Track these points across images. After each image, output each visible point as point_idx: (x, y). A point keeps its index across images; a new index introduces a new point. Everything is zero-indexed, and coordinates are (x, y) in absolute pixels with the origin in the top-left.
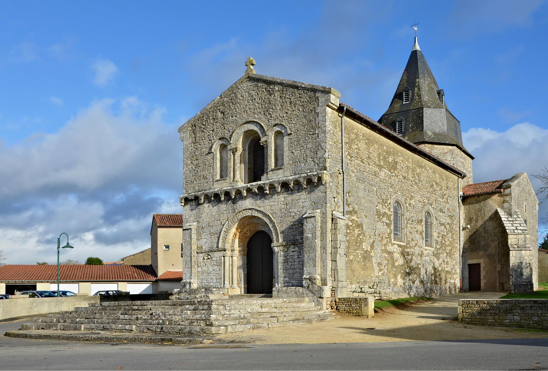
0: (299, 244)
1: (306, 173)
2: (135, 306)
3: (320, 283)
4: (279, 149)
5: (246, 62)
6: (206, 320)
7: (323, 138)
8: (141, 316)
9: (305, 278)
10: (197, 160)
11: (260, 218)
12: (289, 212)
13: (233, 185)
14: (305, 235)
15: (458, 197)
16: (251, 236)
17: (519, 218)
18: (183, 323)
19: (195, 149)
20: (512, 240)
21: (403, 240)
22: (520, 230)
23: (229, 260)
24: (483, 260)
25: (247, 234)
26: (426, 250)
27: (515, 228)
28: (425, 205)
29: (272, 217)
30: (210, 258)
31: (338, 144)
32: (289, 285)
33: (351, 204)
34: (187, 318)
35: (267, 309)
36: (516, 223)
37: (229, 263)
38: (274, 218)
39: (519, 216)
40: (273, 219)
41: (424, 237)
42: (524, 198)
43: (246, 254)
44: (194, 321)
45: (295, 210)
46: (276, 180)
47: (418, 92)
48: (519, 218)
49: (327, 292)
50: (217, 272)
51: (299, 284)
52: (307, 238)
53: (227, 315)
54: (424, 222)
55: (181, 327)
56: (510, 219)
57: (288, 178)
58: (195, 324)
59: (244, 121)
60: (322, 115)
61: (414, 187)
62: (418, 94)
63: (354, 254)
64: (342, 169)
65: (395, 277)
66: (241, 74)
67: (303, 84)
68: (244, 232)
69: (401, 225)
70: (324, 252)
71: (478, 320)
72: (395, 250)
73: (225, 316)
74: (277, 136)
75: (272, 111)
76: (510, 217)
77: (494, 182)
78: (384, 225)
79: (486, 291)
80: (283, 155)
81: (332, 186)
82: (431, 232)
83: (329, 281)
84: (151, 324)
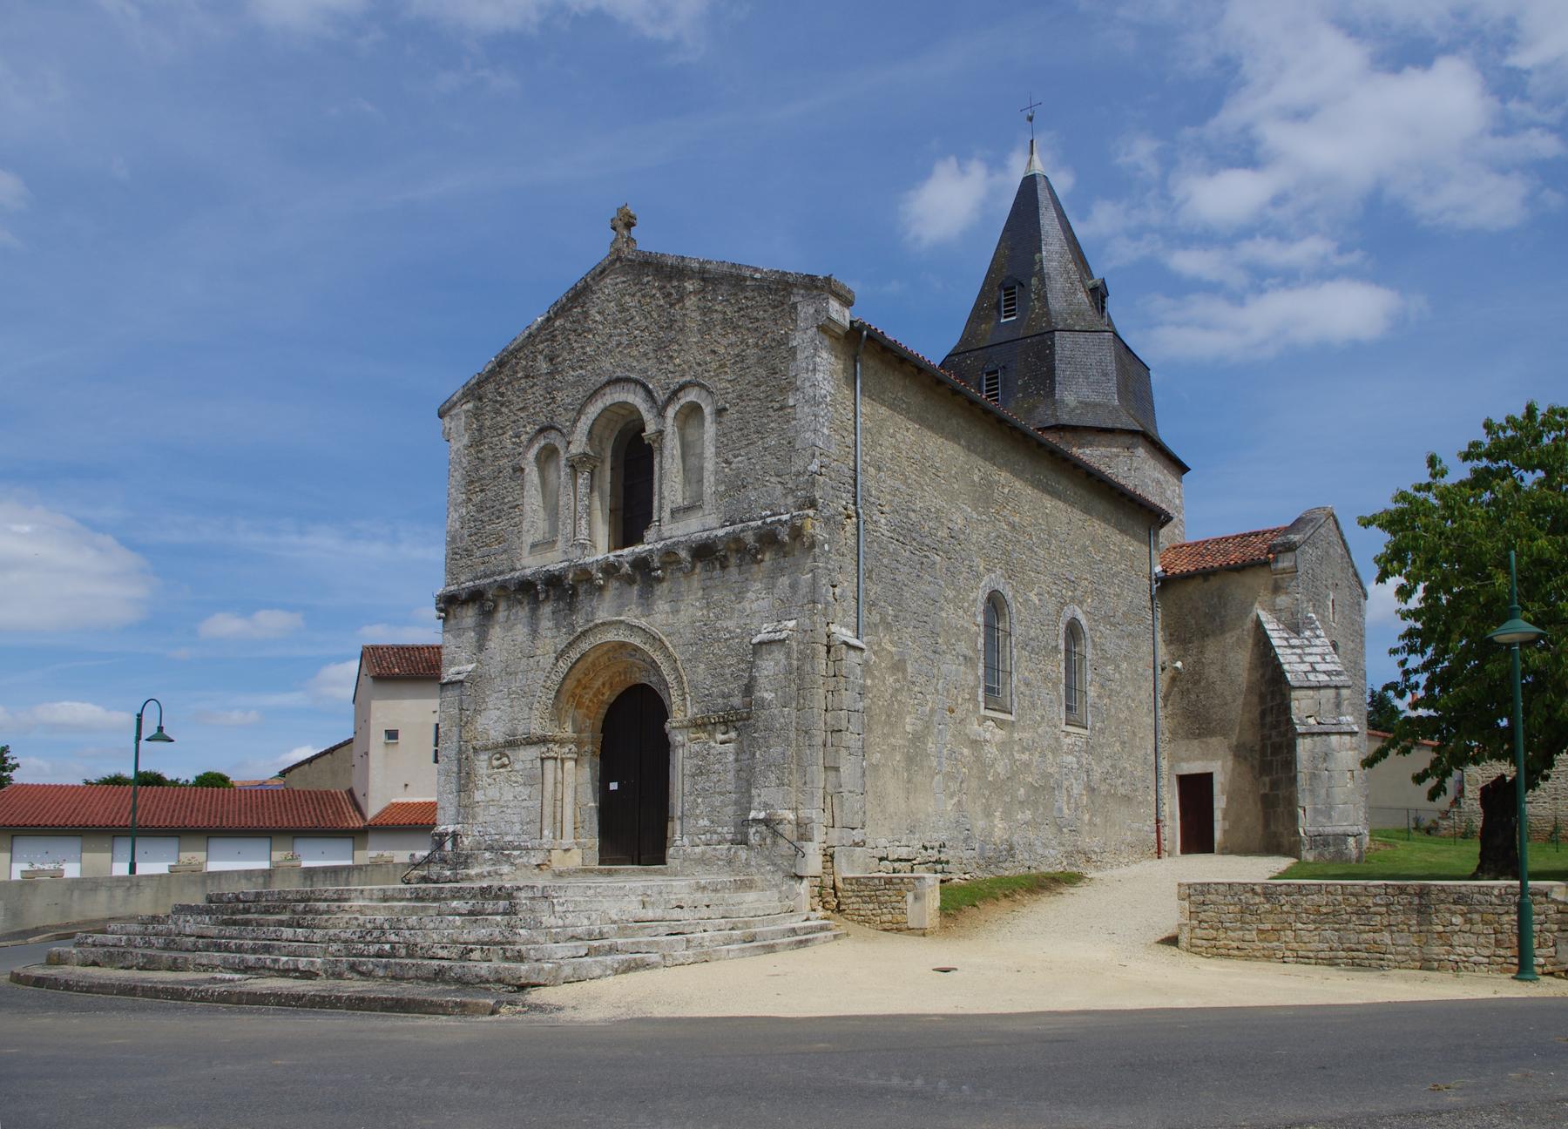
0: (738, 720)
1: (761, 518)
2: (319, 900)
3: (795, 833)
4: (692, 452)
5: (612, 220)
6: (503, 944)
8: (337, 931)
9: (754, 820)
10: (482, 491)
11: (636, 649)
13: (571, 556)
15: (1150, 580)
16: (612, 701)
17: (1318, 637)
18: (444, 953)
19: (477, 462)
20: (1301, 705)
21: (1009, 706)
22: (1324, 672)
23: (556, 769)
24: (1220, 763)
25: (603, 694)
26: (1068, 734)
27: (1309, 668)
28: (1064, 604)
29: (670, 646)
30: (507, 762)
31: (845, 434)
33: (877, 602)
34: (455, 938)
35: (659, 913)
36: (1311, 654)
37: (555, 778)
38: (674, 647)
39: (1318, 632)
40: (671, 649)
41: (1064, 698)
42: (1330, 581)
43: (598, 752)
44: (473, 947)
45: (731, 624)
46: (683, 539)
47: (1040, 290)
48: (1318, 637)
49: (813, 863)
50: (525, 804)
51: (739, 836)
52: (762, 704)
53: (558, 930)
54: (1063, 654)
55: (438, 965)
56: (1294, 642)
57: (715, 533)
58: (476, 955)
59: (604, 379)
60: (806, 354)
61: (1036, 553)
62: (1038, 294)
63: (885, 747)
64: (855, 504)
65: (988, 814)
66: (599, 246)
67: (756, 270)
69: (1004, 661)
71: (1234, 945)
72: (988, 736)
74: (687, 417)
75: (676, 347)
76: (1293, 635)
77: (1244, 535)
78: (960, 665)
79: (1228, 850)
80: (702, 468)
81: (829, 551)
82: (1081, 683)
83: (819, 829)
84: (362, 955)
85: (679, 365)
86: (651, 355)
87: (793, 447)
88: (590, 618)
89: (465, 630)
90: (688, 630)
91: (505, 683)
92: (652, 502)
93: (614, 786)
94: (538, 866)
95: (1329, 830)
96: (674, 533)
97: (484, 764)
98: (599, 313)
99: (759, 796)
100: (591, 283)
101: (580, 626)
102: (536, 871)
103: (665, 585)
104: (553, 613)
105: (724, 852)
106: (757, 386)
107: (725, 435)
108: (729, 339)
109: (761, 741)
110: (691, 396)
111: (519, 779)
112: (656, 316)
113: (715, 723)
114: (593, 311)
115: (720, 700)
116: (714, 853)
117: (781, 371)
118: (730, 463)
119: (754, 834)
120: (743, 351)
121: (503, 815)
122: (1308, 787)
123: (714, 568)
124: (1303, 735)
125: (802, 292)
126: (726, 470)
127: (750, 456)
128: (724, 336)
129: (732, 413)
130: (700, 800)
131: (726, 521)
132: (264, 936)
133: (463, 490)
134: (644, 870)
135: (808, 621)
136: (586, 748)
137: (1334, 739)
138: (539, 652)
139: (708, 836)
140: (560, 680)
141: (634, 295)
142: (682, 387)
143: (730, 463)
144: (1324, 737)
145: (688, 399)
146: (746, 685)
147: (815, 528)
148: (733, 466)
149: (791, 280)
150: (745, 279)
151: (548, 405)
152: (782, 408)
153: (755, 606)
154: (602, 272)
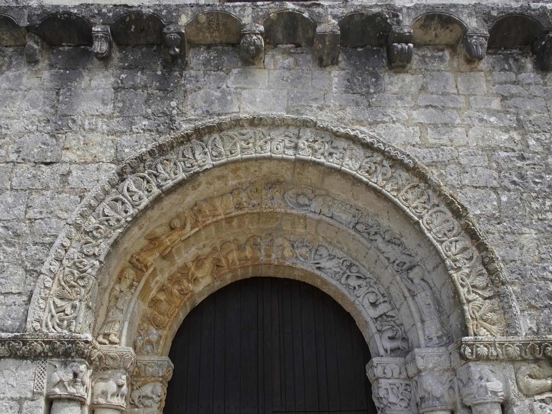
25: (196, 280)
88: (216, 108)
90: (481, 160)
92: (237, 2)
101: (189, 121)
104: (117, 89)
123: (521, 69)
136: (147, 390)
138: (68, 156)
140: (125, 218)
147: (128, 290)
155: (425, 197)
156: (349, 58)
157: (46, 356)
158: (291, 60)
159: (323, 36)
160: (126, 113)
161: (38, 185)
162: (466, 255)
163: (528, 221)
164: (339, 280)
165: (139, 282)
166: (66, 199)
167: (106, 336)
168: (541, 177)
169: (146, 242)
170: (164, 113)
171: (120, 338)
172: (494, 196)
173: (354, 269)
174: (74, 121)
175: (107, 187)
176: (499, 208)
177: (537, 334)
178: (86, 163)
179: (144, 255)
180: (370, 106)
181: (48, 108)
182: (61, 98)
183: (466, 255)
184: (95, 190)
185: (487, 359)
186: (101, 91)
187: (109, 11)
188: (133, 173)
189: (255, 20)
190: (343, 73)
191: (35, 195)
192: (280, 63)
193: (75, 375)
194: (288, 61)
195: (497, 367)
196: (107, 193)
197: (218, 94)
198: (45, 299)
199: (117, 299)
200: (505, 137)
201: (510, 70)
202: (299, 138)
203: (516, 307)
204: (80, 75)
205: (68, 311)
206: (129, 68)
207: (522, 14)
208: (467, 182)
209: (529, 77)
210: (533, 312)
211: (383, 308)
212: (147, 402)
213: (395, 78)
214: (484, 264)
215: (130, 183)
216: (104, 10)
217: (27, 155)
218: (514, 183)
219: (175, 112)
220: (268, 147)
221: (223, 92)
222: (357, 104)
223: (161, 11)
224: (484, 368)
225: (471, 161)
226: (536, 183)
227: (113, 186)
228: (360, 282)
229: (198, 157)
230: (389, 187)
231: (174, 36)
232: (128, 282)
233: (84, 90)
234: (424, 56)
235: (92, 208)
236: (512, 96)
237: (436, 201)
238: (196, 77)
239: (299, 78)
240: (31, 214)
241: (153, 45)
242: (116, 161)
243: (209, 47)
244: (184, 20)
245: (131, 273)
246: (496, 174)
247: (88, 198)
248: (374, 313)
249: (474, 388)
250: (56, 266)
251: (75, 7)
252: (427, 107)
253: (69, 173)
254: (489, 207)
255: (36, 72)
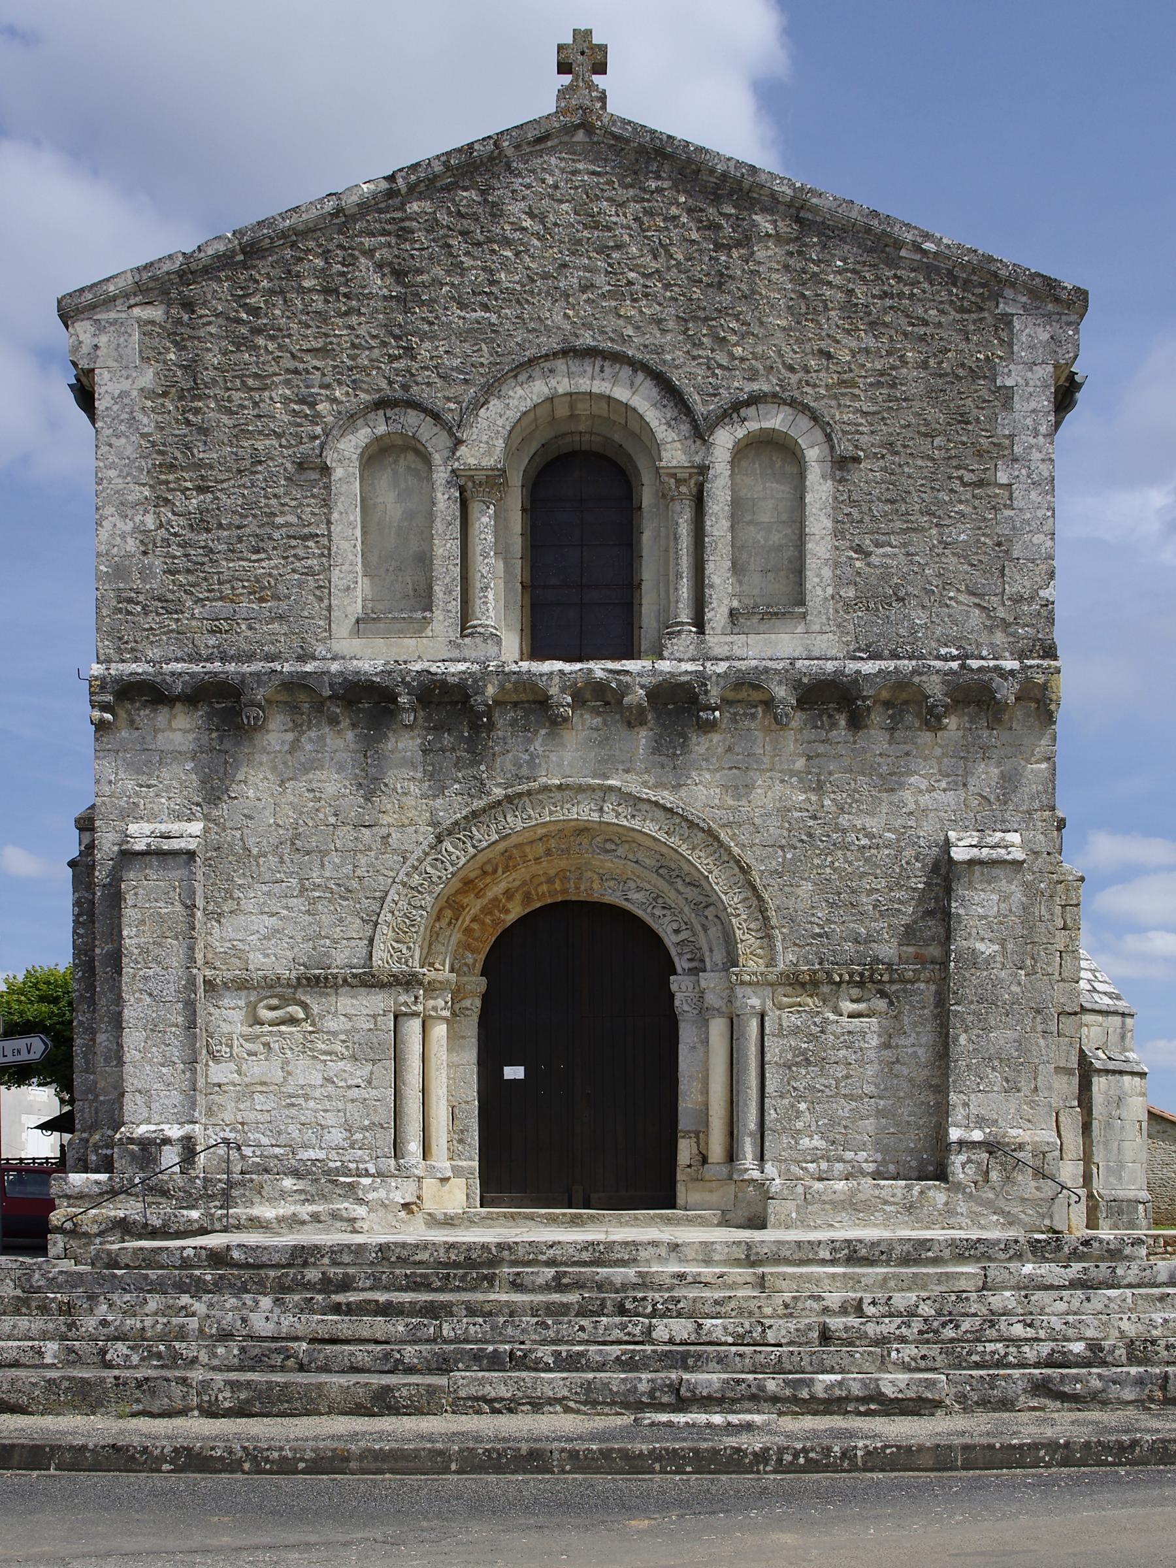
0: (891, 982)
4: (748, 518)
5: (561, 48)
7: (1040, 513)
9: (961, 1143)
10: (201, 490)
12: (836, 830)
14: (959, 944)
25: (507, 912)
30: (302, 1015)
32: (830, 1169)
45: (873, 824)
52: (973, 960)
67: (927, 236)
68: (485, 901)
70: (1039, 1028)
73: (888, 1451)
84: (999, 1364)
85: (742, 359)
86: (671, 325)
87: (1007, 552)
88: (525, 771)
89: (166, 757)
90: (774, 822)
91: (289, 867)
93: (515, 1072)
94: (406, 1206)
95: (1121, 1194)
96: (738, 652)
97: (237, 1016)
98: (531, 215)
99: (966, 1105)
100: (510, 152)
102: (403, 1214)
103: (716, 737)
104: (425, 752)
105: (899, 1192)
106: (926, 435)
107: (853, 503)
108: (859, 339)
109: (970, 1018)
110: (776, 420)
111: (339, 1048)
112: (680, 257)
113: (839, 984)
114: (515, 209)
115: (848, 946)
116: (877, 1192)
117: (978, 420)
118: (868, 554)
119: (963, 1165)
120: (893, 368)
121: (293, 1111)
122: (1103, 1139)
123: (834, 725)
124: (1099, 1072)
125: (1024, 299)
126: (858, 564)
127: (912, 550)
128: (848, 332)
129: (867, 473)
130: (803, 1106)
131: (859, 650)
132: (583, 1336)
133: (144, 478)
134: (661, 1217)
135: (1041, 837)
136: (467, 1003)
137: (1127, 1078)
138: (385, 819)
139: (824, 1165)
141: (622, 205)
142: (754, 400)
143: (868, 554)
144: (1117, 1077)
145: (767, 425)
146: (907, 926)
148: (874, 560)
149: (1003, 273)
150: (899, 244)
151: (393, 358)
152: (981, 484)
153: (925, 800)
154: (539, 140)
155: (717, 855)
156: (658, 718)
157: (391, 985)
158: (599, 720)
159: (630, 708)
160: (437, 777)
161: (361, 847)
162: (748, 903)
163: (806, 875)
164: (645, 910)
165: (457, 920)
166: (391, 859)
167: (432, 965)
168: (828, 836)
169: (461, 885)
170: (474, 777)
171: (444, 965)
172: (780, 853)
173: (660, 901)
174: (386, 785)
175: (427, 850)
176: (783, 865)
177: (795, 965)
178: (403, 826)
179: (460, 897)
180: (675, 768)
181: (357, 771)
182: (369, 761)
183: (748, 903)
184: (418, 852)
185: (750, 984)
186: (409, 754)
187: (414, 680)
188: (449, 835)
189: (563, 690)
190: (651, 733)
191: (359, 856)
192: (588, 723)
193: (416, 998)
194: (597, 721)
195: (759, 989)
196: (427, 854)
197: (526, 757)
198: (384, 943)
199: (438, 935)
200: (802, 797)
201: (822, 727)
202: (604, 801)
203: (779, 946)
204: (385, 736)
205: (404, 951)
206: (434, 728)
207: (833, 681)
208: (757, 841)
209: (840, 734)
210: (796, 949)
211: (684, 935)
212: (467, 1012)
213: (702, 739)
214: (761, 912)
215: (447, 845)
216: (408, 679)
217: (346, 818)
218: (802, 841)
219: (484, 775)
220: (575, 809)
221: (531, 755)
222: (663, 767)
223: (467, 679)
224: (748, 990)
225: (764, 821)
226: (822, 841)
227: (432, 848)
228: (665, 912)
229: (509, 820)
230: (684, 847)
231: (482, 708)
232: (447, 920)
233: (392, 752)
234: (735, 714)
235: (415, 868)
236: (818, 755)
237: (726, 859)
238: (504, 739)
239: (607, 739)
240: (359, 872)
241: (457, 703)
242: (434, 824)
243: (515, 704)
244: (491, 690)
245: (448, 913)
246: (785, 833)
247: (412, 860)
248: (675, 939)
249: (738, 1004)
250: (389, 917)
251: (376, 674)
252: (730, 768)
253: (389, 835)
254: (774, 863)
255: (339, 732)
